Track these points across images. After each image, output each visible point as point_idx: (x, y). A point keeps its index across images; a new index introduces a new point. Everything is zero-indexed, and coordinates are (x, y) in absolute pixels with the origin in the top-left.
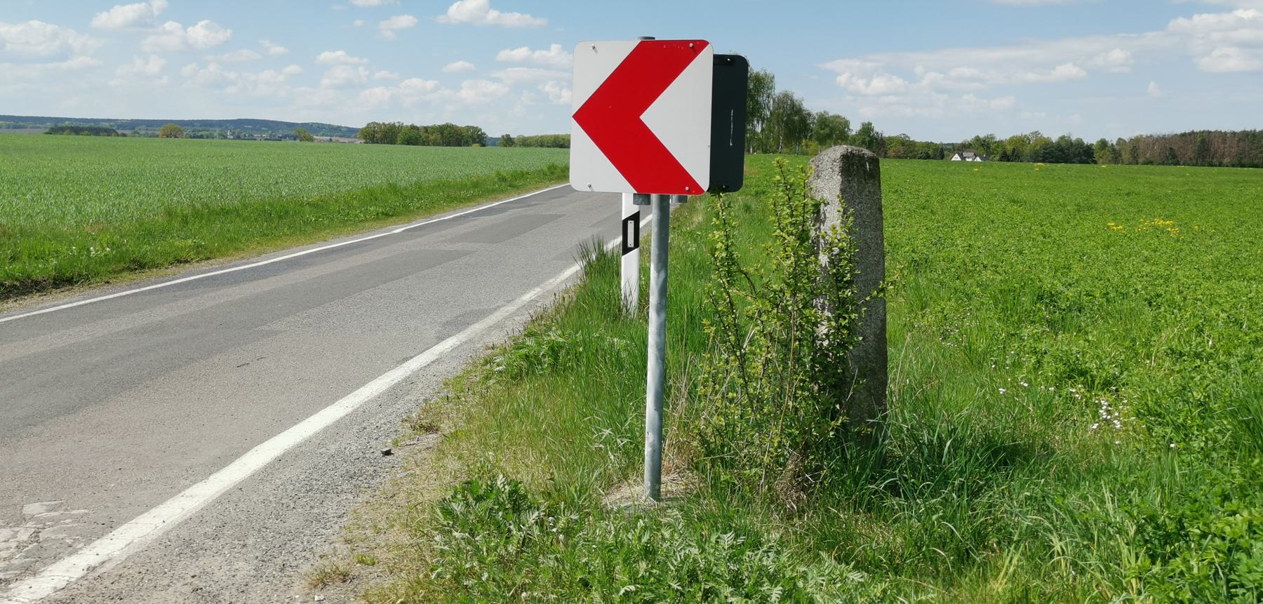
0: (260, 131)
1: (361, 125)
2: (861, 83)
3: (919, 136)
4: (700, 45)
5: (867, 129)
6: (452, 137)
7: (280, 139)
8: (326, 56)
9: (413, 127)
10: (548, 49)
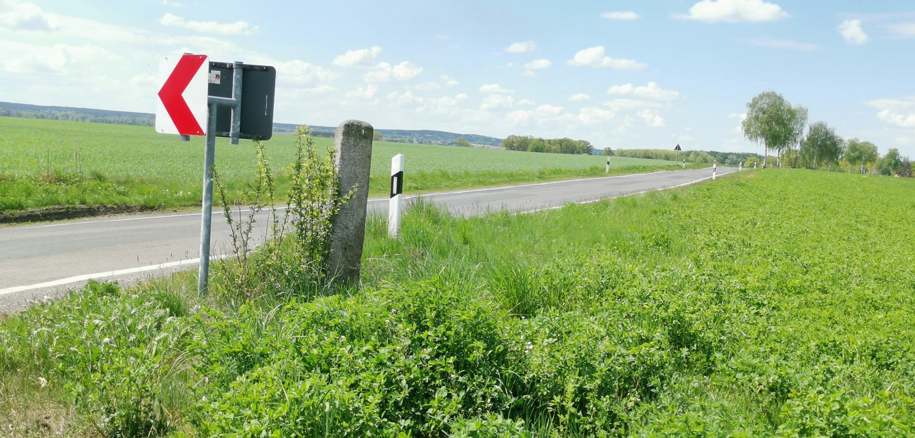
0: (436, 139)
1: (503, 136)
2: (898, 118)
4: (204, 57)
5: (893, 154)
8: (486, 87)
9: (540, 140)
10: (646, 85)
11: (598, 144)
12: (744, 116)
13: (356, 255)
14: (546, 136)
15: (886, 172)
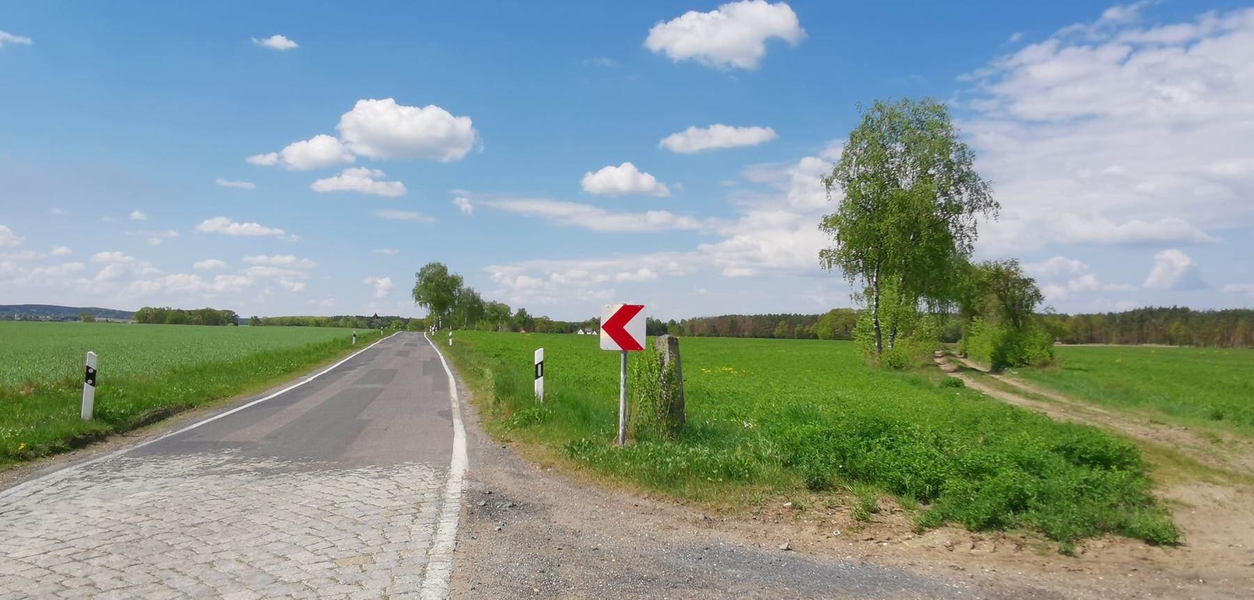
0: (42, 314)
1: (136, 309)
3: (555, 318)
5: (522, 313)
6: (211, 318)
7: (62, 320)
8: (105, 255)
9: (179, 311)
11: (243, 315)
12: (414, 285)
13: (1203, 321)
14: (186, 306)
15: (516, 330)
